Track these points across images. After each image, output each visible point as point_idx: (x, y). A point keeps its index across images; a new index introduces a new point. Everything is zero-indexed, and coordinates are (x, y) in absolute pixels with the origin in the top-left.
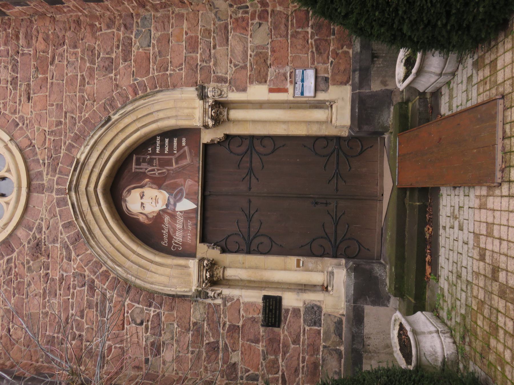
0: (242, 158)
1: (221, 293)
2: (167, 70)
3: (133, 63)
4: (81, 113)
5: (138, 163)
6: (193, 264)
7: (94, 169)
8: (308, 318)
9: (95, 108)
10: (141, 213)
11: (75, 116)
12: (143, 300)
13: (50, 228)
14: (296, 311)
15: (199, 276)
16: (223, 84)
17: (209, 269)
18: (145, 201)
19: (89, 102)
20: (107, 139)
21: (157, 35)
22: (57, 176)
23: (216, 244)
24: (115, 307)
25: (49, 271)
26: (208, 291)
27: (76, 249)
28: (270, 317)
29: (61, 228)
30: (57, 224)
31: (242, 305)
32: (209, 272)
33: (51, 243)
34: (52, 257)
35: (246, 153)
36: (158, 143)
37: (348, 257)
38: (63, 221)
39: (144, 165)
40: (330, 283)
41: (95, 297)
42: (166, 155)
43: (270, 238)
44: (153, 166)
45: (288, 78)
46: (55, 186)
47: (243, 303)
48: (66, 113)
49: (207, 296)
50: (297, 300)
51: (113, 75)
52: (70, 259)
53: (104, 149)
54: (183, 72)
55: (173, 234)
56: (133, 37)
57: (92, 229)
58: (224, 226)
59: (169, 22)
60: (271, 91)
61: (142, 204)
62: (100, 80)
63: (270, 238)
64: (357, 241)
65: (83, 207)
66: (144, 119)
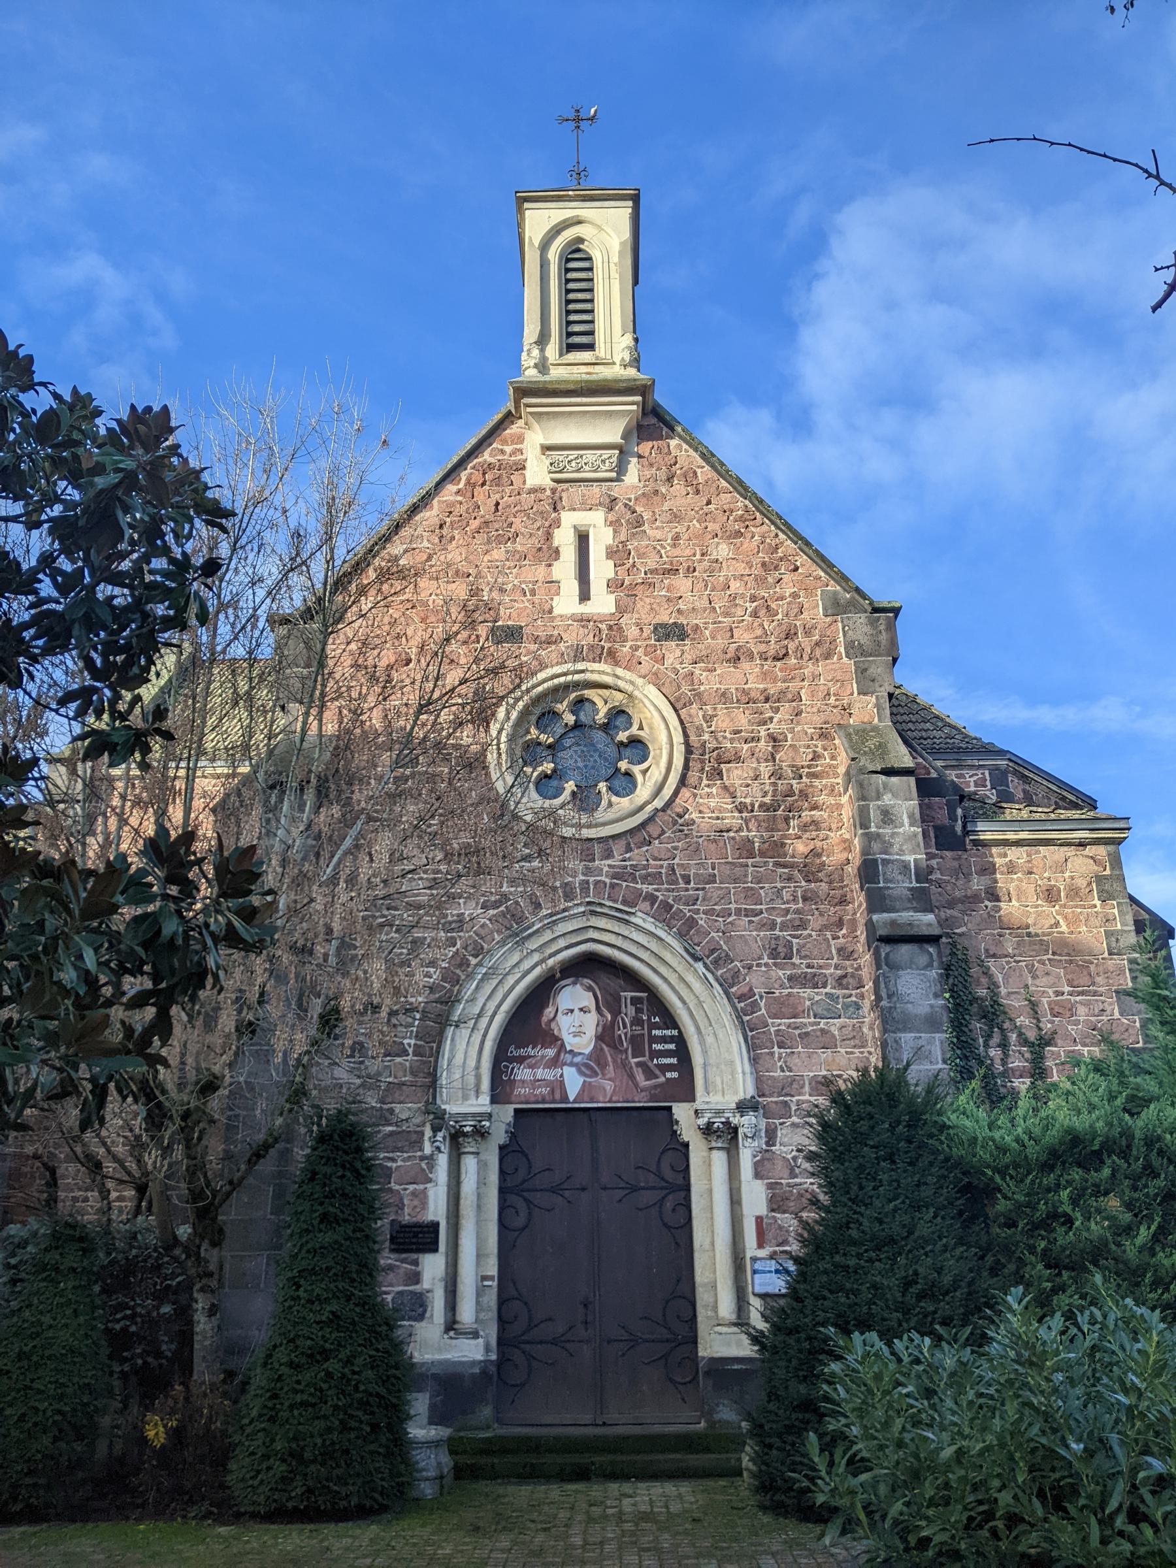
1: (440, 1152)
5: (635, 1001)
6: (482, 1103)
8: (406, 1299)
9: (713, 934)
14: (416, 1278)
16: (764, 1140)
18: (576, 1016)
20: (668, 956)
21: (832, 1028)
22: (608, 881)
23: (513, 1136)
31: (421, 1187)
35: (663, 1179)
36: (668, 1032)
37: (501, 1362)
39: (631, 1011)
40: (461, 1334)
42: (650, 1046)
45: (781, 1249)
46: (592, 879)
48: (703, 889)
49: (436, 1129)
54: (778, 1073)
56: (828, 990)
58: (542, 1150)
59: (855, 1047)
60: (759, 1220)
61: (572, 1011)
66: (702, 1012)
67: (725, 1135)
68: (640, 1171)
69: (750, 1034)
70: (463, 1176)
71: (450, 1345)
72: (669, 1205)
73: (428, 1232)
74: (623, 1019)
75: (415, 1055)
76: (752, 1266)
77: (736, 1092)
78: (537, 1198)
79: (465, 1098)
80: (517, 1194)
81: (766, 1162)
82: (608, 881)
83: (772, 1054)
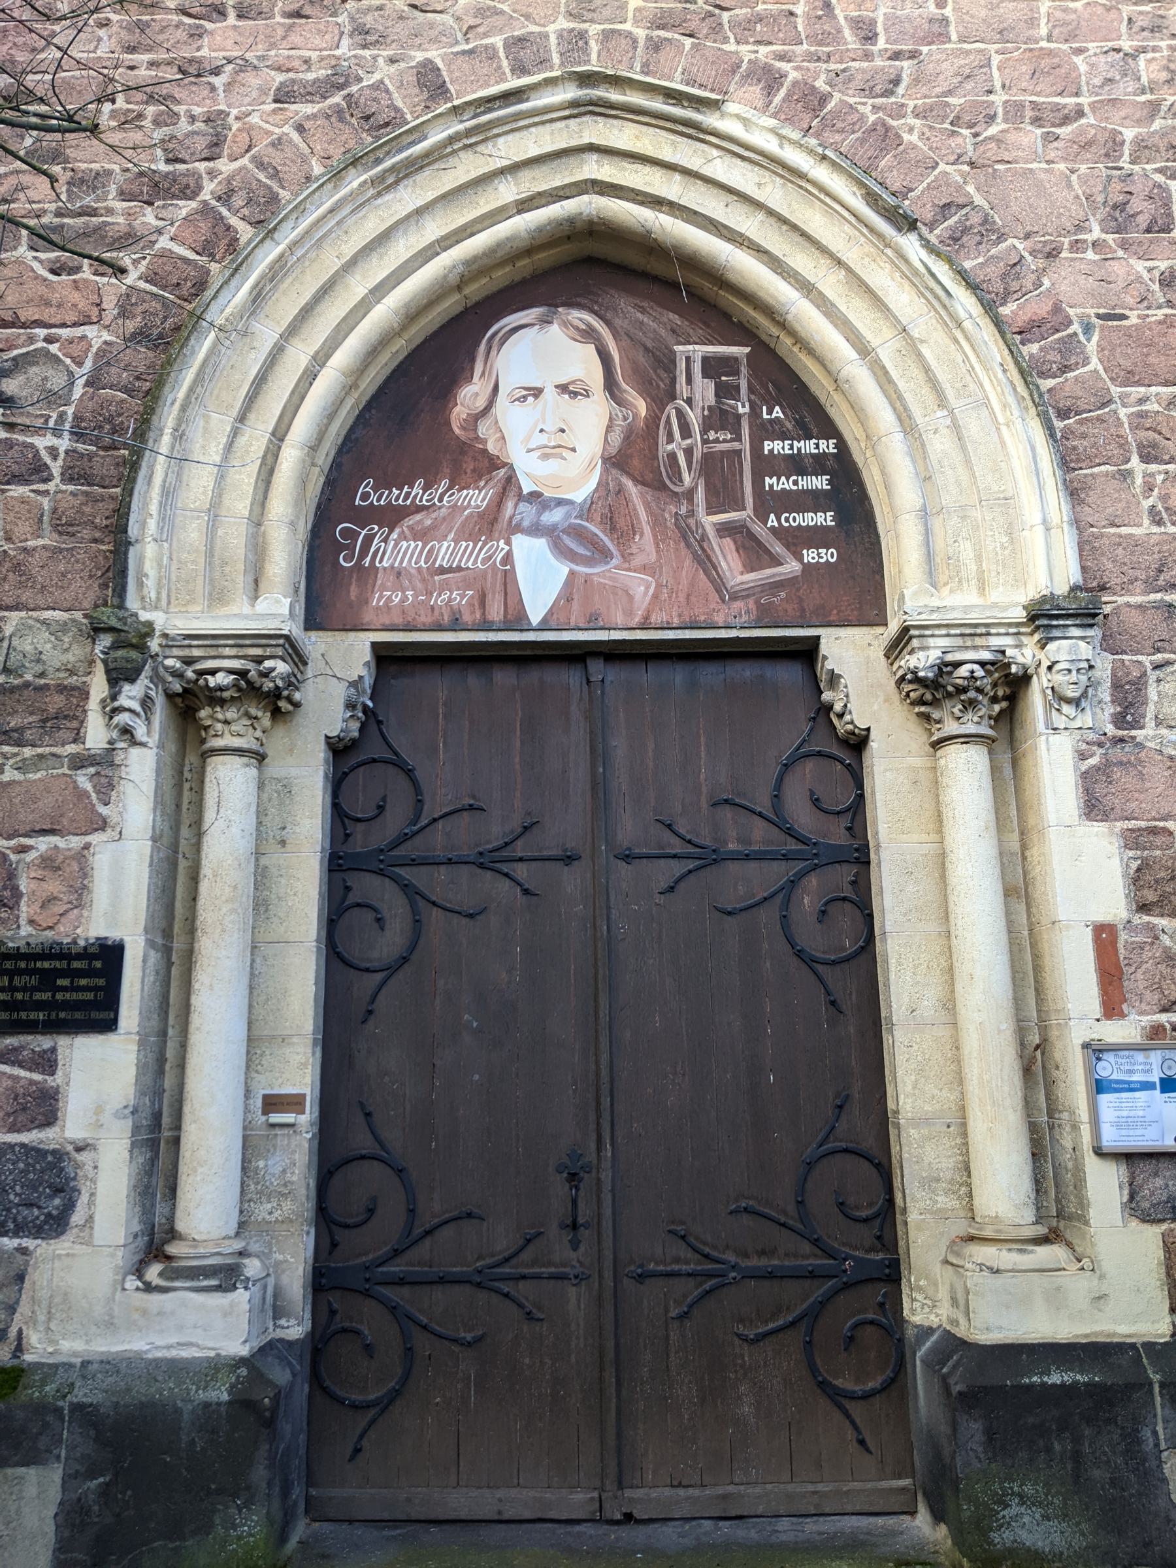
0: (760, 815)
2: (1146, 459)
3: (1161, 313)
4: (917, 116)
6: (276, 609)
7: (677, 177)
10: (496, 389)
11: (901, 90)
12: (106, 403)
13: (417, 13)
14: (44, 1107)
15: (213, 640)
16: (1110, 710)
17: (248, 682)
18: (549, 403)
19: (970, 140)
23: (371, 719)
24: (76, 285)
25: (232, 19)
26: (143, 681)
27: (328, 117)
28: (16, 982)
29: (419, 56)
30: (435, 40)
31: (76, 842)
32: (236, 685)
33: (352, 19)
34: (290, 28)
35: (790, 832)
36: (808, 447)
37: (319, 1344)
38: (449, 65)
39: (705, 391)
41: (119, 205)
43: (405, 960)
44: (704, 431)
46: (594, 29)
47: (87, 847)
48: (914, 55)
49: (118, 676)
50: (99, 1110)
51: (1096, 233)
52: (283, 96)
53: (771, 213)
54: (1144, 528)
55: (411, 528)
57: (419, 177)
60: (1104, 937)
61: (537, 392)
62: (1069, 186)
63: (405, 960)
64: (395, 1395)
65: (510, 137)
66: (917, 372)
67: (988, 699)
68: (727, 813)
69: (1059, 424)
70: (209, 815)
71: (144, 1312)
72: (808, 901)
73: (89, 973)
74: (680, 414)
75: (67, 477)
76: (1090, 1069)
77: (1021, 581)
78: (436, 881)
79: (217, 597)
80: (381, 873)
81: (1117, 773)
82: (641, 33)
83: (1126, 475)
